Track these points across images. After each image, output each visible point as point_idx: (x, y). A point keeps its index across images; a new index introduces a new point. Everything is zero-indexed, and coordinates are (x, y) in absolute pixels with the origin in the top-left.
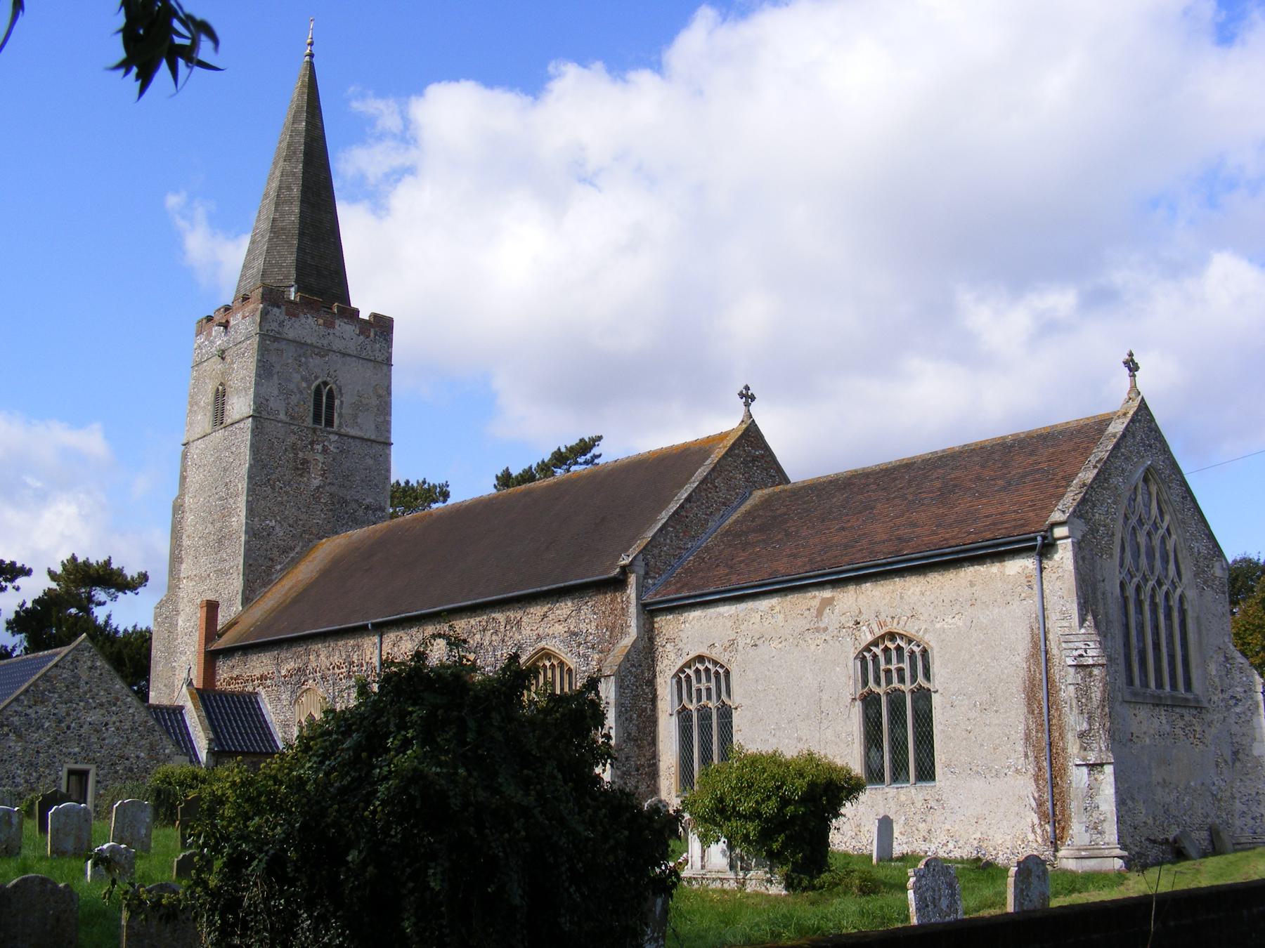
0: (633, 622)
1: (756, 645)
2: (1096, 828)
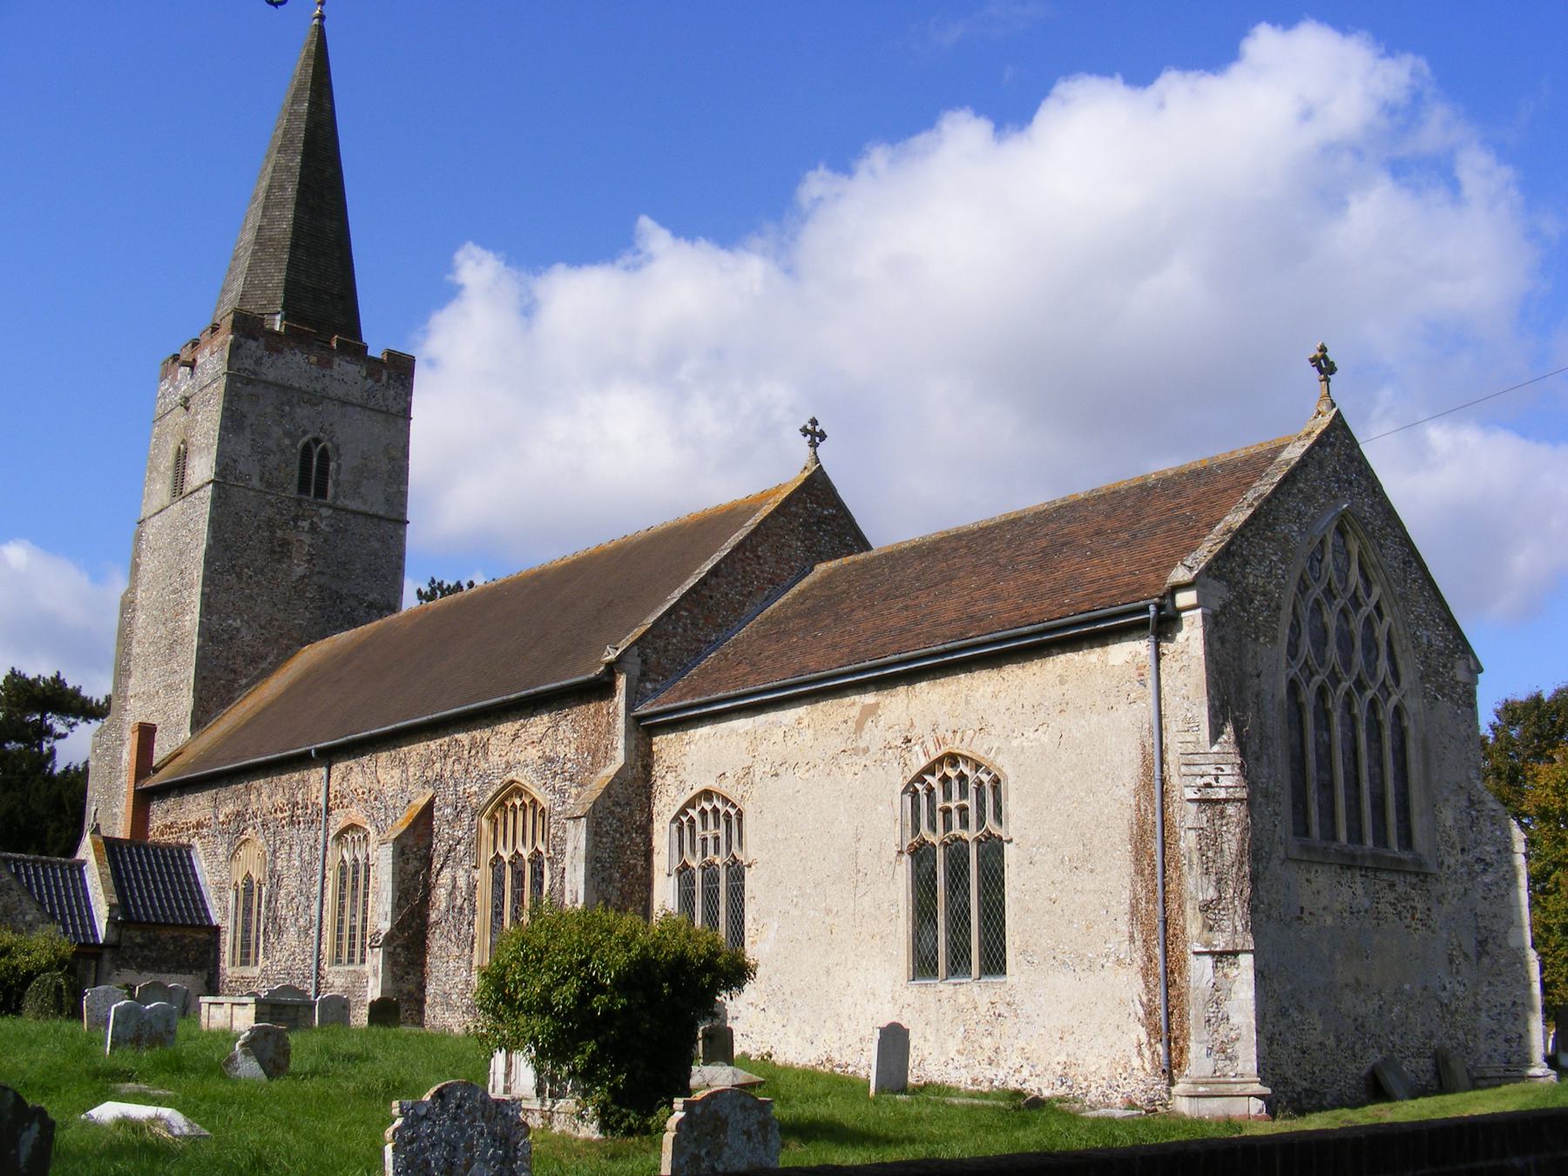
0: (620, 743)
1: (777, 775)
2: (1223, 1050)
